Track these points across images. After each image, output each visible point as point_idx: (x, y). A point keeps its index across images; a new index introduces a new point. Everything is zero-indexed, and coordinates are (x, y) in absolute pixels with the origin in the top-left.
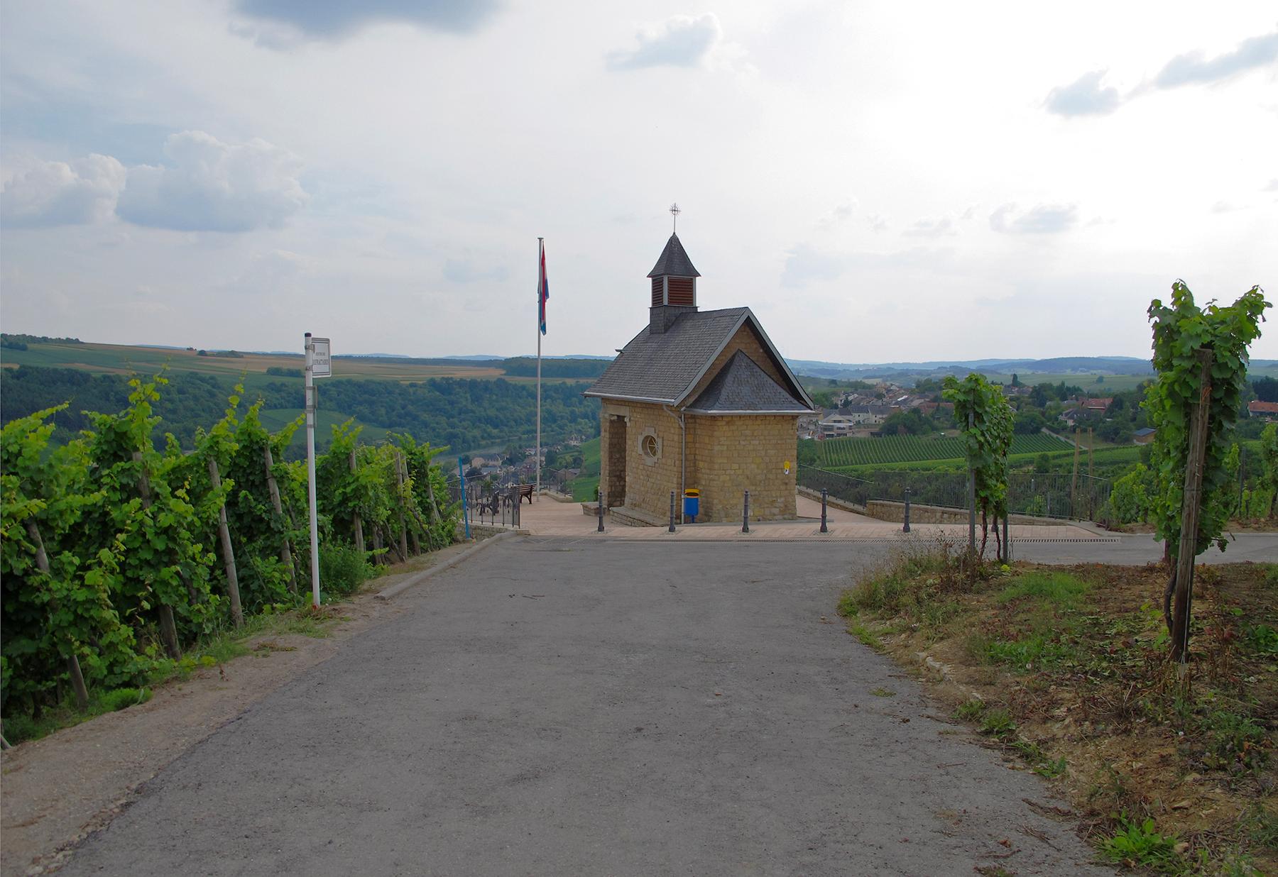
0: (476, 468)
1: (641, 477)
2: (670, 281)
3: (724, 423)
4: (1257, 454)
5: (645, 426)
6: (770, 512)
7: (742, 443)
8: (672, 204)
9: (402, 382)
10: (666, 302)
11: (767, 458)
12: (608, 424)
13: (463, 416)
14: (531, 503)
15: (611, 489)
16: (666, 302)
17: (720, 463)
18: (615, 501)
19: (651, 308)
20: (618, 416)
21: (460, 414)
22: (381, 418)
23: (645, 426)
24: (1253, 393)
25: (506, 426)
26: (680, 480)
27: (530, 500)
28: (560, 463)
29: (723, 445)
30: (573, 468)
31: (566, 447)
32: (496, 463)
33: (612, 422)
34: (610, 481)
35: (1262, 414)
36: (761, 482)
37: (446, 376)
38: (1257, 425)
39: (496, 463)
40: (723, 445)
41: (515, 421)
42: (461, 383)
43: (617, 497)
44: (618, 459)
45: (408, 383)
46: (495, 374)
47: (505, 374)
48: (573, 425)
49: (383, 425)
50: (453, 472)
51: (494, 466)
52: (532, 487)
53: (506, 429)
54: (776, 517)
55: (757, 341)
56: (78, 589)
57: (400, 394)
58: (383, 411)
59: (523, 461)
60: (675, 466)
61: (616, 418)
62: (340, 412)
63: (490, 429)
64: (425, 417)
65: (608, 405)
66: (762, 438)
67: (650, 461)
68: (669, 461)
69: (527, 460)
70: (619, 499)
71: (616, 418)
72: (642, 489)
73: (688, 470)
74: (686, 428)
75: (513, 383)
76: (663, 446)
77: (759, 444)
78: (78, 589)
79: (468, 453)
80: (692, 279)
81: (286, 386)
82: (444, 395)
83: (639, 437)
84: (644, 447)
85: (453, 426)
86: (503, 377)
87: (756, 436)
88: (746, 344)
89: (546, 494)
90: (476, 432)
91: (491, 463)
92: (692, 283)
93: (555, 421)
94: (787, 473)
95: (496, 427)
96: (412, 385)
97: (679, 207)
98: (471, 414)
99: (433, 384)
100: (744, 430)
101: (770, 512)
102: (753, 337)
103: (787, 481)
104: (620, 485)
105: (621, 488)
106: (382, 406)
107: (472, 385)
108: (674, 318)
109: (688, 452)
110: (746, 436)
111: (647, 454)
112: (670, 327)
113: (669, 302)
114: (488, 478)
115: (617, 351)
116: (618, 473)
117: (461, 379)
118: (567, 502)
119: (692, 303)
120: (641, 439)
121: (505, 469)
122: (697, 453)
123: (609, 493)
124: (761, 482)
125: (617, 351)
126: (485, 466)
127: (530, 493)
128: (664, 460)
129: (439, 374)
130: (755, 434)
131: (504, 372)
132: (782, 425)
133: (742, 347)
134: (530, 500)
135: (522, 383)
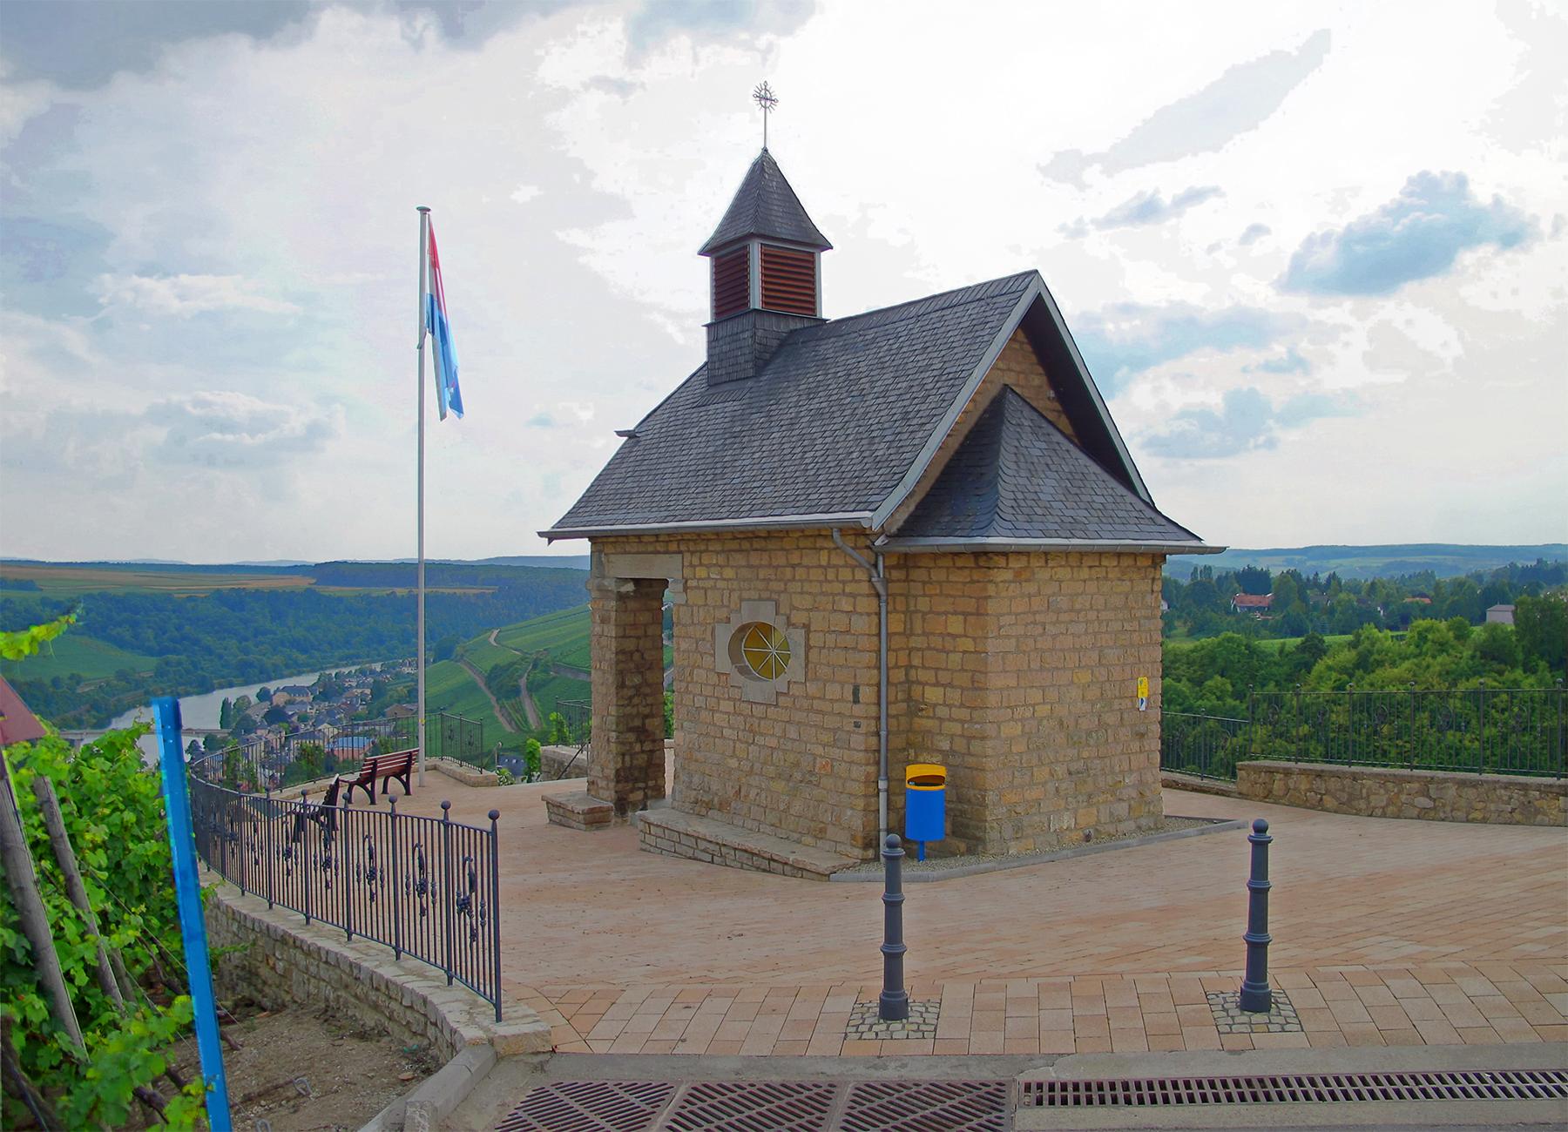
0: (278, 706)
1: (726, 732)
2: (767, 258)
3: (1008, 575)
4: (1272, 655)
5: (741, 600)
6: (1111, 814)
7: (1051, 629)
8: (759, 82)
9: (176, 595)
10: (756, 301)
11: (1104, 671)
12: (613, 603)
13: (260, 638)
14: (408, 793)
15: (623, 762)
16: (756, 301)
17: (1001, 690)
18: (632, 791)
19: (708, 326)
20: (637, 581)
21: (256, 636)
22: (147, 644)
23: (741, 600)
24: (1236, 585)
25: (318, 650)
26: (874, 740)
27: (406, 785)
28: (391, 697)
29: (1008, 637)
30: (408, 702)
31: (398, 676)
32: (305, 699)
33: (622, 597)
34: (620, 742)
35: (1249, 609)
36: (1089, 734)
37: (236, 587)
38: (1247, 621)
39: (305, 699)
40: (1008, 637)
41: (330, 643)
42: (257, 595)
43: (636, 780)
44: (637, 688)
45: (185, 596)
46: (303, 583)
47: (315, 584)
48: (405, 646)
49: (150, 652)
50: (247, 712)
51: (302, 702)
52: (410, 755)
53: (316, 654)
54: (1122, 827)
55: (1041, 370)
56: (1049, 398)
57: (174, 612)
58: (150, 633)
59: (341, 694)
60: (856, 701)
61: (630, 587)
62: (90, 637)
63: (296, 654)
64: (208, 640)
65: (612, 558)
66: (1092, 615)
67: (757, 690)
68: (833, 691)
69: (347, 694)
70: (641, 785)
71: (630, 587)
72: (733, 763)
73: (893, 710)
74: (887, 595)
75: (327, 594)
76: (808, 648)
77: (1086, 633)
78: (1049, 398)
79: (266, 685)
80: (812, 254)
81: (11, 602)
82: (233, 610)
83: (720, 629)
84: (734, 655)
85: (246, 651)
86: (313, 586)
87: (1079, 611)
88: (1019, 373)
89: (435, 768)
90: (278, 659)
91: (298, 699)
92: (813, 262)
93: (381, 642)
94: (1143, 708)
95: (304, 651)
96: (190, 599)
97: (776, 91)
98: (272, 636)
99: (220, 597)
100: (1054, 594)
101: (1111, 814)
102: (1034, 358)
103: (1142, 730)
104: (643, 752)
105: (645, 756)
106: (149, 627)
107: (272, 597)
108: (775, 343)
109: (892, 663)
110: (1059, 611)
111: (743, 671)
112: (767, 363)
113: (767, 298)
114: (295, 719)
115: (620, 434)
116: (637, 723)
117: (257, 590)
118: (487, 785)
119: (814, 310)
120: (724, 635)
121: (316, 707)
122: (916, 662)
123: (617, 771)
124: (1089, 734)
125: (620, 434)
126: (290, 702)
127: (406, 769)
128: (812, 689)
129: (227, 584)
130: (1077, 606)
131: (314, 581)
132: (1131, 581)
133: (1009, 379)
134: (406, 785)
135: (339, 594)
